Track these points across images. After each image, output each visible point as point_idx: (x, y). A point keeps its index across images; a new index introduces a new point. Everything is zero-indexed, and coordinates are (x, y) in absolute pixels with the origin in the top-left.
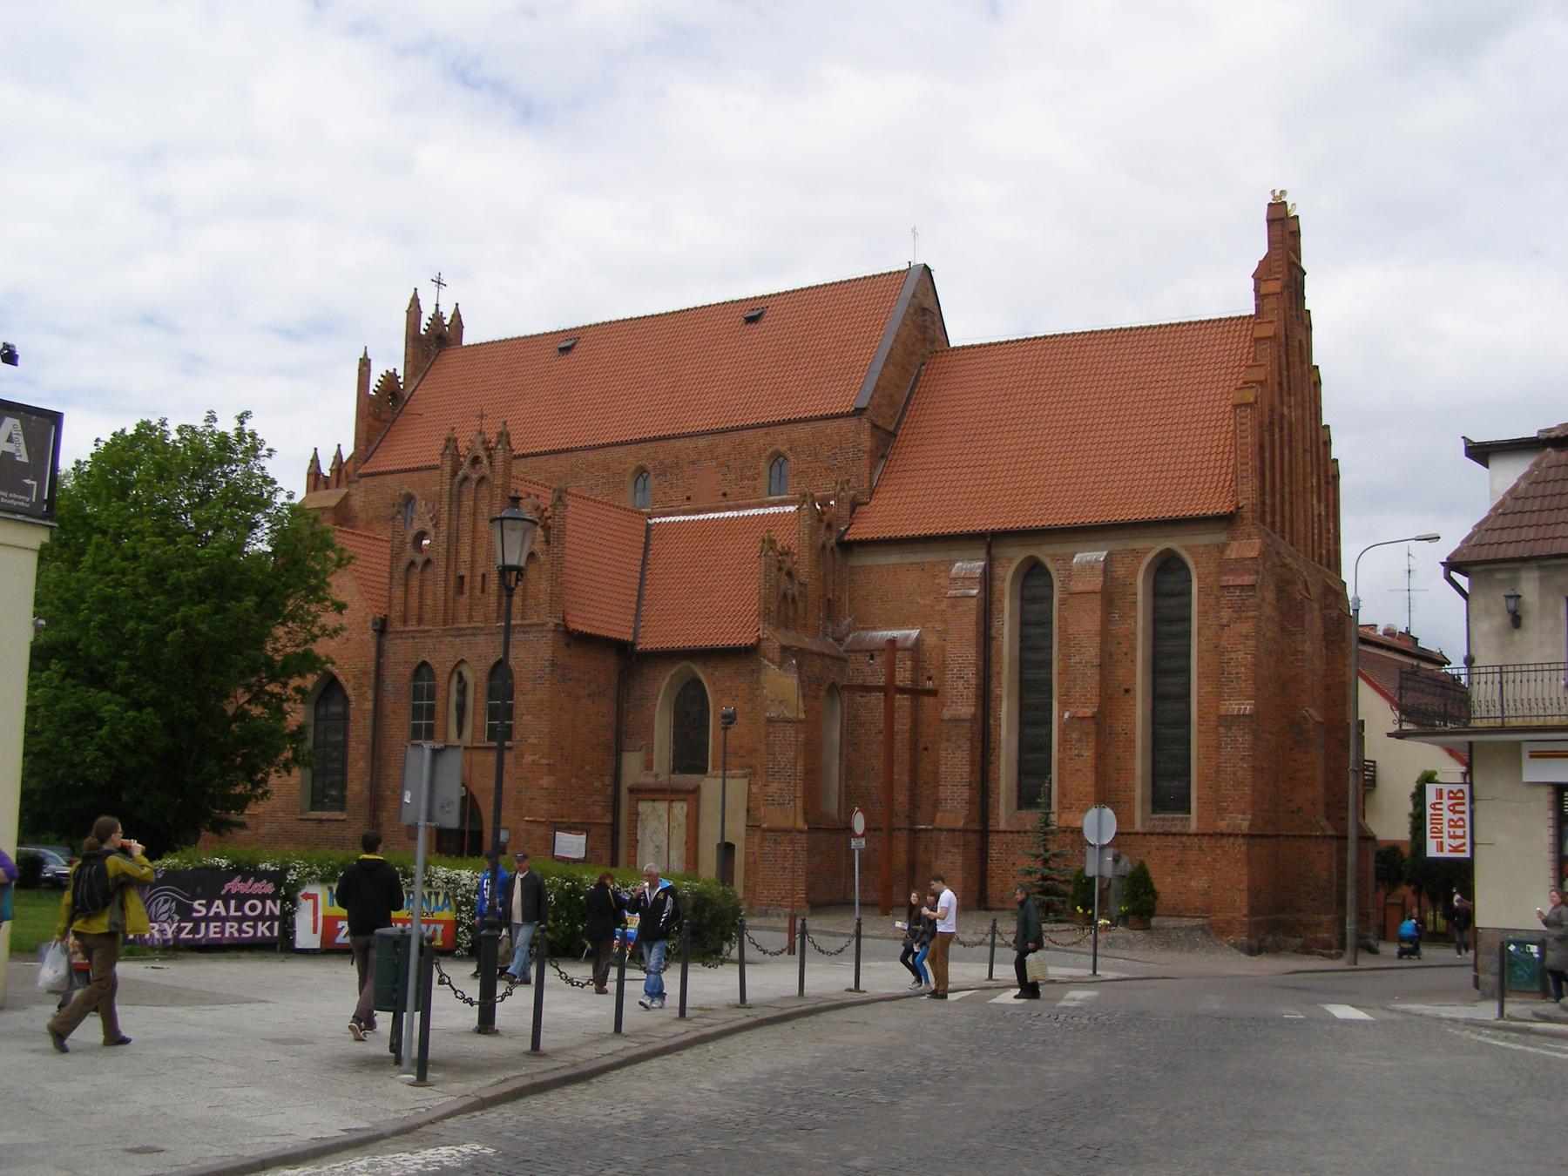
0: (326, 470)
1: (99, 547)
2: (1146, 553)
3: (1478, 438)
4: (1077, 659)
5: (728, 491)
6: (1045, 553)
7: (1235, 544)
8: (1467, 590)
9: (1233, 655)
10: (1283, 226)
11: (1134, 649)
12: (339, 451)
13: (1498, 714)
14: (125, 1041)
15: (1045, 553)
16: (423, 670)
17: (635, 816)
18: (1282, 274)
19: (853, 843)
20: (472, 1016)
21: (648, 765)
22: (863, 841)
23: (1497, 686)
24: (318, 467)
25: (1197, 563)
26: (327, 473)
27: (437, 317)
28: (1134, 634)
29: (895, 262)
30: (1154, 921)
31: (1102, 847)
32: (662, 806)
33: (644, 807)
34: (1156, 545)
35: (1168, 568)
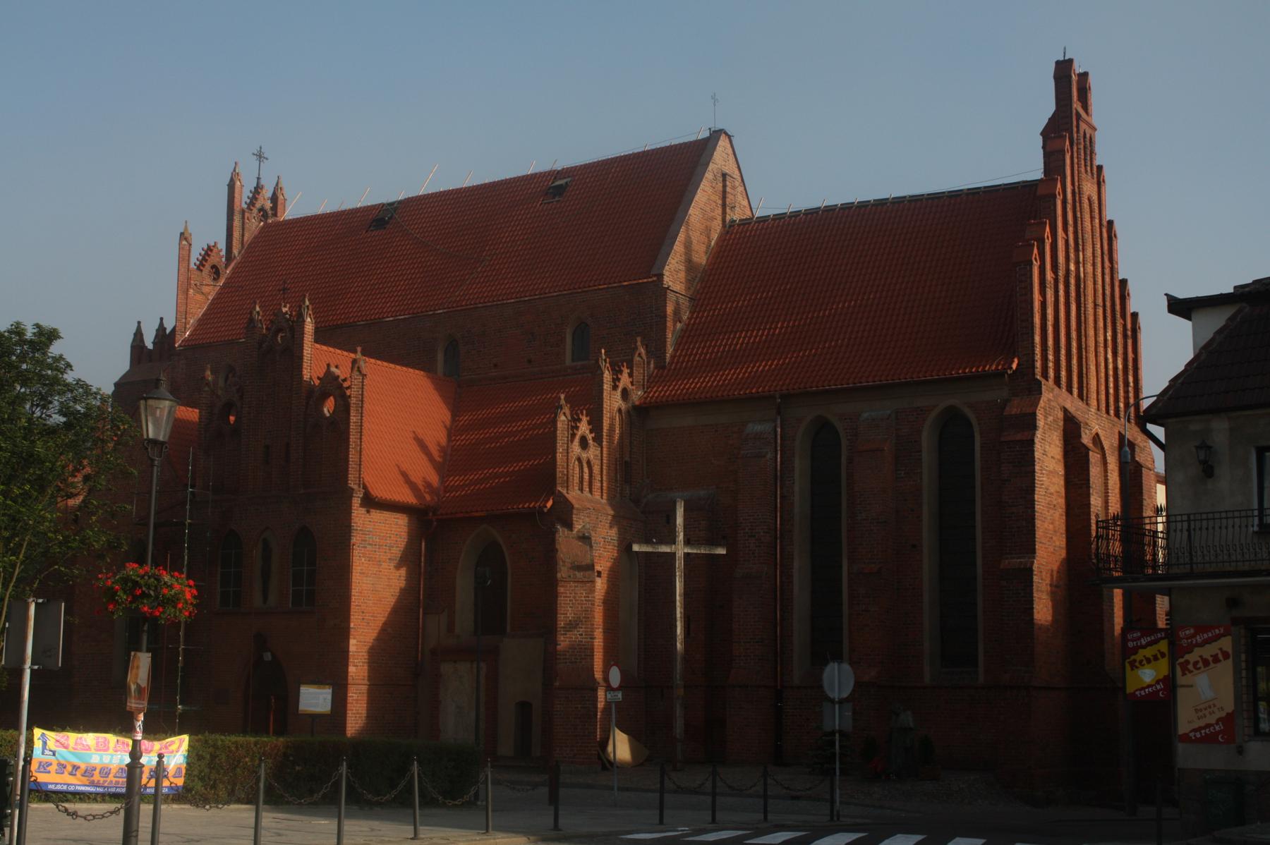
0: (149, 342)
3: (1181, 295)
8: (1163, 440)
10: (1070, 85)
12: (161, 324)
13: (1187, 560)
16: (591, 491)
18: (1066, 129)
20: (762, 816)
23: (1185, 534)
24: (142, 341)
26: (150, 346)
27: (258, 190)
29: (1053, 66)
31: (841, 702)
33: (447, 668)
35: (824, 439)
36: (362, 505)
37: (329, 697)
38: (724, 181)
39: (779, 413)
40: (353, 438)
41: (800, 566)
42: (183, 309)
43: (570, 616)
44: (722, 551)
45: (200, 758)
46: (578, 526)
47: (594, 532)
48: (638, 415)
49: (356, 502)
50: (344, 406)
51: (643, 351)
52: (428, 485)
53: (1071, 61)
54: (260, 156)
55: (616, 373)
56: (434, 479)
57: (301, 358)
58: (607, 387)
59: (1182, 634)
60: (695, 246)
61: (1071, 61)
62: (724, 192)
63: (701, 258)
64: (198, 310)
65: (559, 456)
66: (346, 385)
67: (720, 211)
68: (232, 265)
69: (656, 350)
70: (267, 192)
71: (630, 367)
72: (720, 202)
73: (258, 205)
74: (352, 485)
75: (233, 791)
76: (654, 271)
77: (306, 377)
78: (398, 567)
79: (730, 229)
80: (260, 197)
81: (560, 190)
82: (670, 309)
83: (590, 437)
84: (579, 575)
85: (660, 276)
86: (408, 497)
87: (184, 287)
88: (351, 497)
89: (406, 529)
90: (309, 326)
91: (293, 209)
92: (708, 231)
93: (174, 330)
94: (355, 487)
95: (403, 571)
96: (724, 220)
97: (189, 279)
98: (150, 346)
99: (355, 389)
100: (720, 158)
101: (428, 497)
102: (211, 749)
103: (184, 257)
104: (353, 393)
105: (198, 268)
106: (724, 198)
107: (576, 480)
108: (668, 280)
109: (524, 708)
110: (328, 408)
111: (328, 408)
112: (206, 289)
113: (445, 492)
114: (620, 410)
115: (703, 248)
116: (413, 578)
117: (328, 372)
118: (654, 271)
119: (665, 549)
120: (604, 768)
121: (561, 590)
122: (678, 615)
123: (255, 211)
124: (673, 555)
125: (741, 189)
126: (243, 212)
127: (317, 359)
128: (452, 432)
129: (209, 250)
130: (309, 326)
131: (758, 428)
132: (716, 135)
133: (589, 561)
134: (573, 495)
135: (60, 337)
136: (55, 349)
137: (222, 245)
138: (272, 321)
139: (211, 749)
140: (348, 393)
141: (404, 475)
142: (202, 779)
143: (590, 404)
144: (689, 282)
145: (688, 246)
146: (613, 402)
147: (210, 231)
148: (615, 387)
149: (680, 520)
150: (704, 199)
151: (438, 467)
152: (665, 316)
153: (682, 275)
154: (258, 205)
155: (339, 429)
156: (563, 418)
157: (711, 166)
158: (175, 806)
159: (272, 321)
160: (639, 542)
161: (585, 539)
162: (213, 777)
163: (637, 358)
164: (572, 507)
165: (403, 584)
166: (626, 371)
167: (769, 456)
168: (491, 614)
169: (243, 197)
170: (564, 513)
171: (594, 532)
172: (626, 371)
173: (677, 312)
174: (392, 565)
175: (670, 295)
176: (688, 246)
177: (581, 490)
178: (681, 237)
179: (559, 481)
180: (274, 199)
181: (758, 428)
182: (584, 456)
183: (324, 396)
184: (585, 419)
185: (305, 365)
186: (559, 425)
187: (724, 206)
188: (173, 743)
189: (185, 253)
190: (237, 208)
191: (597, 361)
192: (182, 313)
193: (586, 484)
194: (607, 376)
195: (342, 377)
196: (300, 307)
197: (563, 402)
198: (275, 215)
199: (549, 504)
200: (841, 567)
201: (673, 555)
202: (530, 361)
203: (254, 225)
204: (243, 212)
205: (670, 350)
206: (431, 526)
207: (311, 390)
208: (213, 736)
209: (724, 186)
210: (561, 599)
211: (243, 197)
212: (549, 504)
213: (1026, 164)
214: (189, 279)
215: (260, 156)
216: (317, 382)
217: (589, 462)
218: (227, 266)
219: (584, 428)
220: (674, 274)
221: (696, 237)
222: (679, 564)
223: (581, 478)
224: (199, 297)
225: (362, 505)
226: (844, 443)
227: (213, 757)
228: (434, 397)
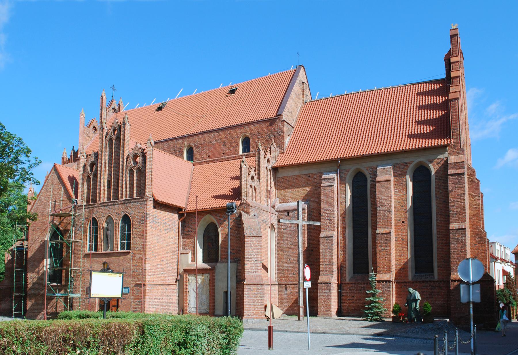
2: (410, 164)
7: (452, 157)
39: (339, 167)
51: (275, 144)
54: (113, 89)
59: (391, 320)
72: (302, 93)
73: (112, 106)
107: (250, 195)
120: (476, 189)
121: (246, 240)
134: (249, 201)
148: (265, 157)
150: (296, 90)
157: (298, 78)
179: (243, 194)
193: (254, 197)
210: (246, 245)
215: (113, 89)
217: (255, 188)
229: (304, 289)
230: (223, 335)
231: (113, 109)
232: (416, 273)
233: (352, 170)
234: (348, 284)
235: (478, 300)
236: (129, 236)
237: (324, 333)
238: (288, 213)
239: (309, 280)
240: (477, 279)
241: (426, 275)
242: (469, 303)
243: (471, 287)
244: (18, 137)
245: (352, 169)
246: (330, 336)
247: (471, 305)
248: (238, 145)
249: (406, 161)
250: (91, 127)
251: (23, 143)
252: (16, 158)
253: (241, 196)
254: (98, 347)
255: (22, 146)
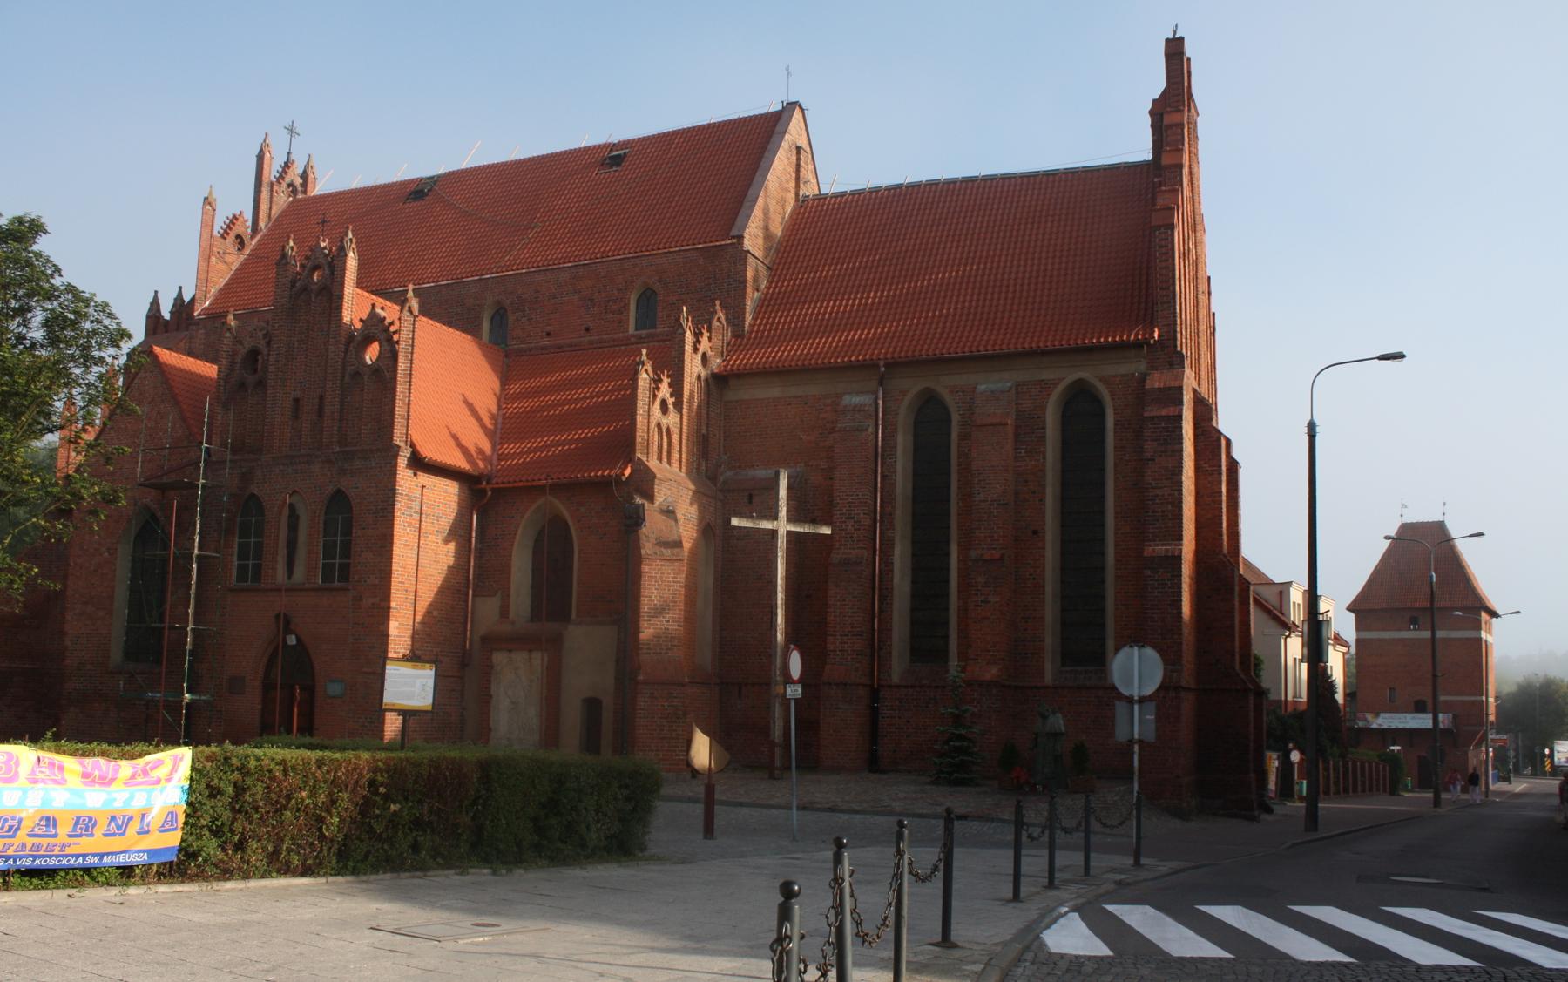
0: (166, 314)
1: (100, 346)
2: (1056, 384)
4: (982, 496)
5: (548, 329)
6: (946, 385)
7: (1156, 375)
9: (1158, 492)
10: (1175, 51)
11: (1044, 487)
14: (955, 946)
15: (946, 385)
16: (669, 463)
17: (487, 672)
18: (1172, 113)
19: (789, 691)
21: (504, 612)
22: (799, 689)
25: (1112, 394)
26: (167, 316)
27: (287, 165)
28: (1043, 470)
30: (663, 792)
32: (520, 657)
33: (499, 658)
34: (1067, 375)
35: (930, 418)
36: (409, 466)
37: (431, 683)
38: (798, 153)
39: (881, 384)
40: (401, 388)
41: (901, 554)
42: (203, 276)
43: (656, 600)
44: (826, 531)
45: (214, 792)
46: (659, 499)
47: (675, 502)
48: (717, 382)
49: (402, 462)
50: (391, 354)
51: (721, 315)
52: (481, 451)
53: (1182, 39)
54: (292, 131)
55: (698, 335)
56: (486, 446)
57: (341, 297)
58: (688, 348)
60: (772, 215)
61: (1182, 39)
62: (798, 165)
63: (777, 230)
64: (220, 280)
65: (639, 418)
66: (392, 329)
67: (793, 184)
68: (258, 237)
69: (735, 319)
70: (298, 168)
71: (709, 330)
74: (398, 439)
75: (276, 852)
76: (734, 232)
77: (346, 319)
78: (446, 541)
79: (802, 203)
80: (290, 171)
81: (617, 161)
82: (750, 274)
83: (671, 401)
84: (667, 552)
85: (741, 238)
86: (458, 461)
87: (206, 254)
88: (396, 456)
89: (456, 498)
90: (352, 262)
91: (323, 185)
92: (782, 202)
93: (193, 299)
94: (402, 444)
95: (452, 546)
96: (797, 194)
97: (211, 246)
98: (167, 316)
99: (404, 331)
100: (794, 132)
101: (481, 465)
102: (236, 776)
103: (207, 223)
104: (403, 339)
105: (222, 237)
106: (798, 171)
108: (748, 244)
109: (592, 706)
110: (371, 354)
111: (371, 354)
112: (229, 258)
113: (499, 460)
114: (699, 377)
115: (778, 219)
116: (462, 553)
117: (373, 314)
118: (734, 232)
119: (766, 525)
121: (645, 568)
122: (779, 602)
123: (284, 185)
124: (774, 533)
125: (811, 167)
126: (272, 185)
127: (355, 306)
128: (503, 399)
129: (234, 219)
130: (352, 262)
131: (857, 400)
132: (792, 106)
133: (676, 538)
134: (653, 463)
135: (46, 232)
136: (42, 245)
137: (248, 215)
138: (307, 258)
139: (236, 776)
140: (395, 338)
141: (455, 437)
142: (216, 833)
143: (670, 364)
144: (767, 250)
145: (766, 212)
146: (693, 367)
147: (237, 200)
148: (696, 350)
149: (783, 493)
151: (490, 434)
152: (745, 282)
153: (760, 241)
154: (288, 179)
155: (384, 377)
156: (644, 375)
157: (787, 136)
158: (162, 888)
159: (307, 258)
160: (740, 515)
161: (669, 513)
162: (238, 826)
163: (715, 324)
164: (654, 476)
165: (451, 560)
166: (706, 334)
167: (871, 430)
168: (553, 596)
169: (272, 170)
170: (644, 482)
171: (675, 502)
172: (706, 334)
173: (756, 279)
174: (440, 538)
175: (750, 259)
176: (766, 212)
177: (660, 460)
178: (760, 201)
179: (638, 447)
180: (304, 176)
181: (857, 400)
182: (664, 421)
183: (367, 340)
184: (666, 381)
185: (345, 306)
186: (641, 383)
187: (798, 179)
188: (160, 763)
189: (209, 218)
190: (265, 180)
191: (678, 320)
192: (203, 281)
194: (689, 337)
195: (388, 321)
196: (342, 241)
197: (644, 358)
198: (305, 192)
199: (628, 472)
200: (948, 555)
201: (774, 533)
202: (587, 329)
203: (283, 199)
204: (272, 185)
205: (749, 318)
206: (483, 494)
207: (351, 337)
208: (241, 750)
209: (798, 159)
210: (645, 580)
211: (272, 170)
212: (628, 472)
213: (1137, 146)
214: (211, 246)
215: (292, 131)
216: (358, 325)
217: (668, 430)
218: (252, 238)
219: (665, 390)
220: (753, 240)
221: (773, 206)
222: (782, 543)
223: (660, 446)
224: (222, 266)
225: (409, 466)
226: (955, 418)
227: (240, 790)
228: (483, 363)
229: (786, 702)
230: (625, 792)
231: (290, 185)
232: (1063, 665)
233: (910, 396)
234: (898, 686)
235: (1150, 736)
236: (347, 549)
237: (831, 810)
238: (751, 496)
239: (800, 681)
240: (1149, 690)
241: (35, 857)
242: (1131, 741)
243: (1136, 707)
244: (99, 299)
245: (911, 387)
246: (846, 817)
247: (1136, 748)
248: (626, 307)
249: (1047, 375)
250: (231, 238)
251: (111, 316)
252: (86, 348)
253: (634, 451)
254: (420, 802)
255: (107, 322)
